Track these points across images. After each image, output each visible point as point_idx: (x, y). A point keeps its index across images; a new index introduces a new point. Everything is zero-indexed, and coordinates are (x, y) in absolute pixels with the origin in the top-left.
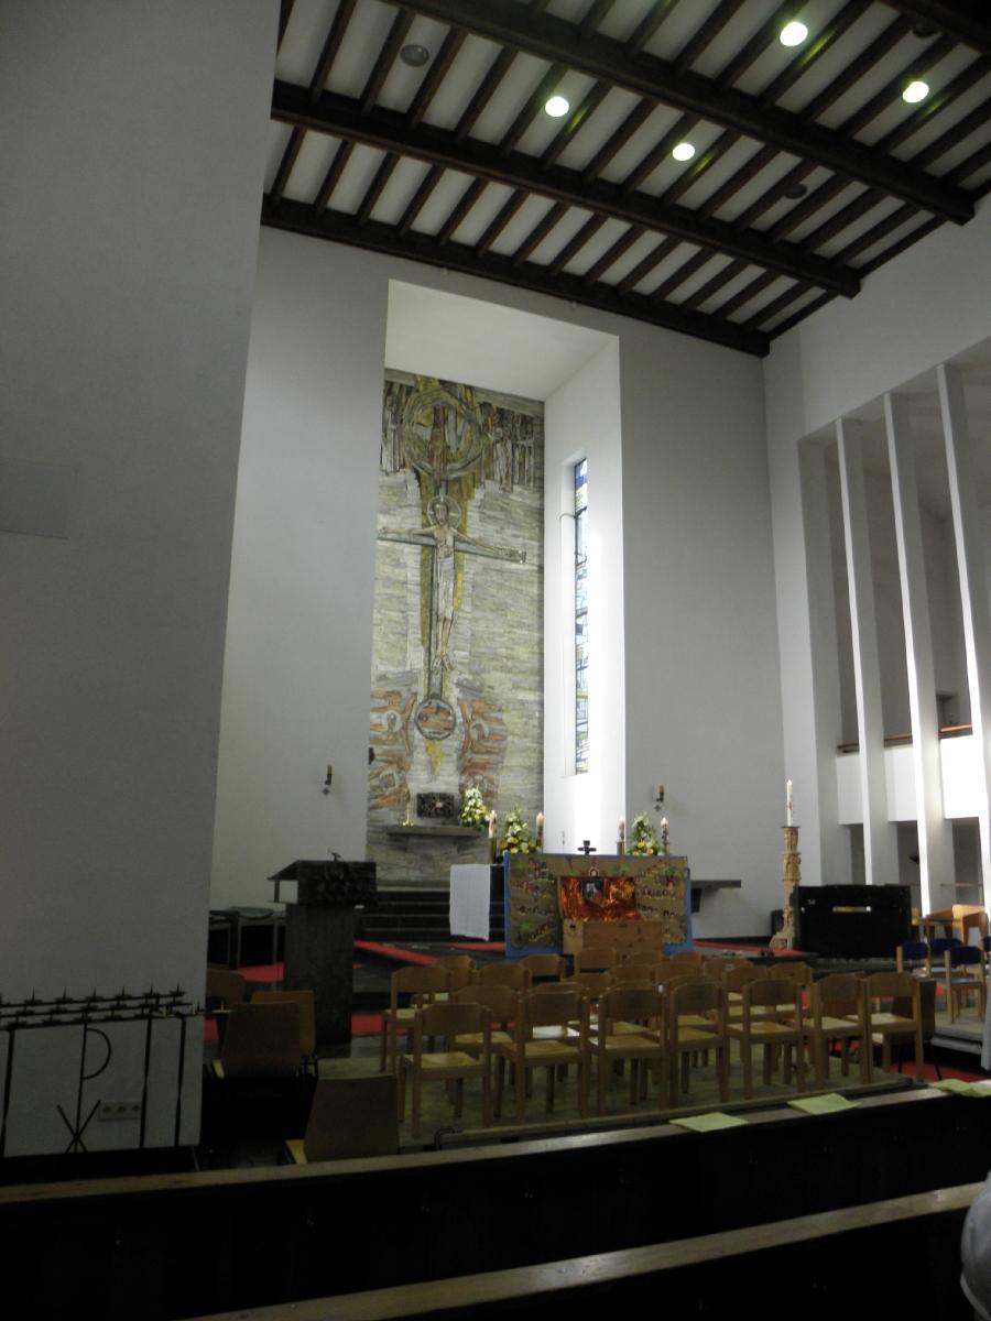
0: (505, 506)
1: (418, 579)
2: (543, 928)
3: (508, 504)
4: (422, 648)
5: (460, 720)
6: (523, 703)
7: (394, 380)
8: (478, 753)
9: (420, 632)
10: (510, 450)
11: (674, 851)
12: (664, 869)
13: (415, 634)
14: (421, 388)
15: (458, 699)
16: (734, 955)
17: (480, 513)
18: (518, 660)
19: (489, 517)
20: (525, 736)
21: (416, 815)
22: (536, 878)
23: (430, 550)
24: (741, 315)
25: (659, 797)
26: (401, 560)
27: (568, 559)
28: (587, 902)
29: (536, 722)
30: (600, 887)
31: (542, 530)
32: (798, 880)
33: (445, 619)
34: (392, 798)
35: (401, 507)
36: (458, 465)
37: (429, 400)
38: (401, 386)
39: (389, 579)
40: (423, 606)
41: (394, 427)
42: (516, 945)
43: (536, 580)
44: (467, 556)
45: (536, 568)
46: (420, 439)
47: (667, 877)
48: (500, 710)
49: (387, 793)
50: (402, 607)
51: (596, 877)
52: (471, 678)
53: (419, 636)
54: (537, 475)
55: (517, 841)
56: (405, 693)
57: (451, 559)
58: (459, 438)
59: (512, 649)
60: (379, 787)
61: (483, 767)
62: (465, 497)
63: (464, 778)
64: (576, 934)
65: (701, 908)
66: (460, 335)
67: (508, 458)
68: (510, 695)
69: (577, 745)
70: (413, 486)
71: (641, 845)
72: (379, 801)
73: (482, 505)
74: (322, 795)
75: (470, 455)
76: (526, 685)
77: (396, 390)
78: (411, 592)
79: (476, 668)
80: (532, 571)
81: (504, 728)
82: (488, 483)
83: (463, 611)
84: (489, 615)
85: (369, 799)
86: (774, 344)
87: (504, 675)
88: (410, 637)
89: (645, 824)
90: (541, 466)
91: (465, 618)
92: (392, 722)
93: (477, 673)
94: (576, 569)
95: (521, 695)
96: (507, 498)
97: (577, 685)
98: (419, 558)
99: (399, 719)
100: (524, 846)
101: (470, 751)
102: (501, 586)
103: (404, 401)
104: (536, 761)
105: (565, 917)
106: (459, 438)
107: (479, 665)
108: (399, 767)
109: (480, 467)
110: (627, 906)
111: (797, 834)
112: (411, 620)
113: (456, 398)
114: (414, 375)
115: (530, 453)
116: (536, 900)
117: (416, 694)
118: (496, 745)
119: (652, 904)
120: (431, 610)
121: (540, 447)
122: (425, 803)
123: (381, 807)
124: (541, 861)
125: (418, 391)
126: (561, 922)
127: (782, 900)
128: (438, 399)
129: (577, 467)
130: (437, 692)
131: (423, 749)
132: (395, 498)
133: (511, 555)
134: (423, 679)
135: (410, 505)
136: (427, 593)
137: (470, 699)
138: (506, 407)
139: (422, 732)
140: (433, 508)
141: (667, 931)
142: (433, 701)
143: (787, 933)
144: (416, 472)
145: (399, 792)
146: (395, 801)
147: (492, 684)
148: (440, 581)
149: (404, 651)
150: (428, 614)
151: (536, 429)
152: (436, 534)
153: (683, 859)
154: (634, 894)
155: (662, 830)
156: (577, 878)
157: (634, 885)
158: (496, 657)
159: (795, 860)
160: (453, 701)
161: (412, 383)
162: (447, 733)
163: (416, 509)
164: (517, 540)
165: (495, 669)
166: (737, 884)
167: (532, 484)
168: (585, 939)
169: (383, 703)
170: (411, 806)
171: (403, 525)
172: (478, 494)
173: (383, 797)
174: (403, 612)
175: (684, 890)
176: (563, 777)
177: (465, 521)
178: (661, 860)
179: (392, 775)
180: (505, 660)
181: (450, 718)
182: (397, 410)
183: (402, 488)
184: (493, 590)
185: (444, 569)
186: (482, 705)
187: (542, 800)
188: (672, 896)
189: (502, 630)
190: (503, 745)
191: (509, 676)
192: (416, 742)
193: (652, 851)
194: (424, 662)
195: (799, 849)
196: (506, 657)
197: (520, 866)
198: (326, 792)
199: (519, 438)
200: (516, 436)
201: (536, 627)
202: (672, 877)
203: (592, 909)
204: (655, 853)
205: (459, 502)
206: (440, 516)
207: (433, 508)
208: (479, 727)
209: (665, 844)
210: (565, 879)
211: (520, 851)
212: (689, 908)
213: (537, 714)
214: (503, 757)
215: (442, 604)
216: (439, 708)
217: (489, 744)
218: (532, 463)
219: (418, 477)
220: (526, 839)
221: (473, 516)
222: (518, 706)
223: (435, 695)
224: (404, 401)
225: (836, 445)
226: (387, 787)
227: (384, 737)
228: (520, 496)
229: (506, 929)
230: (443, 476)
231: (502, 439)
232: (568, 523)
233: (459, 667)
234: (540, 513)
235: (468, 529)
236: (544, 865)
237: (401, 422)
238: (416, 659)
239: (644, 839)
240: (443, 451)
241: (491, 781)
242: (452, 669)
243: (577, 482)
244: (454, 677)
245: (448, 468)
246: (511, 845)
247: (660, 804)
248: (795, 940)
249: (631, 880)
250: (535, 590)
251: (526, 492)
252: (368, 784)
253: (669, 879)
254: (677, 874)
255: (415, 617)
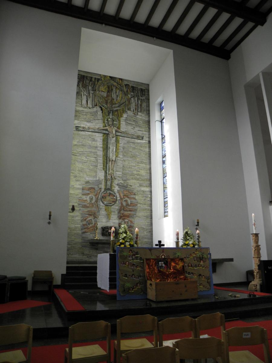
0: (135, 120)
1: (102, 146)
2: (137, 286)
3: (136, 119)
4: (103, 171)
5: (119, 198)
6: (143, 191)
7: (93, 76)
8: (126, 211)
9: (102, 165)
10: (136, 100)
11: (203, 245)
12: (199, 254)
13: (100, 166)
14: (103, 79)
15: (118, 190)
16: (235, 297)
17: (125, 122)
18: (142, 176)
19: (129, 124)
20: (145, 204)
21: (101, 235)
22: (133, 260)
23: (106, 136)
24: (219, 42)
25: (197, 224)
26: (95, 139)
27: (158, 136)
28: (159, 271)
29: (149, 199)
30: (166, 263)
31: (149, 128)
32: (260, 257)
33: (112, 160)
34: (91, 229)
35: (95, 120)
36: (117, 105)
37: (106, 83)
38: (95, 78)
39: (90, 146)
40: (104, 156)
41: (93, 92)
42: (122, 294)
43: (148, 146)
44: (120, 137)
45: (148, 142)
46: (102, 96)
47: (200, 258)
48: (135, 194)
49: (89, 227)
50: (95, 156)
51: (164, 259)
52: (123, 182)
53: (102, 167)
54: (147, 109)
55: (124, 242)
56: (96, 187)
57: (114, 138)
58: (117, 96)
59: (139, 171)
60: (86, 225)
61: (128, 216)
62: (120, 116)
63: (120, 221)
64: (152, 288)
65: (217, 270)
66: (115, 55)
67: (136, 103)
68: (139, 189)
69: (164, 206)
70: (100, 113)
71: (187, 243)
72: (86, 230)
73: (126, 119)
74: (48, 224)
75: (122, 102)
76: (144, 185)
77: (93, 80)
78: (99, 150)
79: (125, 178)
80: (146, 143)
81: (136, 201)
82: (129, 112)
83: (119, 157)
84: (129, 159)
85: (82, 229)
86: (233, 55)
87: (136, 181)
88: (99, 167)
89: (189, 233)
90: (148, 106)
91: (120, 160)
92: (91, 199)
93: (125, 180)
94: (162, 140)
95: (143, 189)
96: (136, 117)
97: (164, 183)
98: (102, 138)
99: (94, 198)
100: (127, 244)
101: (123, 210)
102: (134, 148)
103: (96, 83)
104: (149, 214)
105: (148, 279)
106: (117, 96)
107: (126, 177)
108: (94, 216)
109: (126, 106)
110: (183, 271)
111: (258, 237)
112: (99, 161)
113: (116, 82)
114: (100, 75)
115: (144, 101)
116: (133, 271)
117: (101, 188)
118: (133, 208)
119: (191, 271)
120: (107, 157)
121: (148, 99)
122: (105, 231)
123: (87, 232)
124: (136, 251)
125: (102, 80)
126: (146, 282)
127: (254, 266)
128: (109, 83)
129: (161, 104)
130: (109, 188)
131: (104, 210)
132: (93, 117)
133: (138, 137)
134: (103, 183)
135: (99, 119)
136: (105, 151)
137: (122, 190)
138: (135, 86)
139: (103, 203)
140: (107, 120)
141: (201, 284)
142: (108, 191)
143: (256, 282)
144: (101, 108)
145: (94, 226)
146: (92, 230)
147: (131, 185)
148: (111, 146)
149: (96, 172)
150: (106, 158)
151: (146, 93)
152: (108, 130)
153: (208, 249)
154: (183, 266)
155: (197, 235)
156: (155, 259)
157: (184, 262)
158: (133, 175)
159: (258, 248)
160: (116, 191)
161: (99, 78)
162: (113, 203)
163: (101, 120)
164: (137, 131)
165: (132, 179)
166: (231, 260)
167: (145, 112)
168: (156, 292)
169: (88, 192)
170: (99, 231)
171: (96, 126)
172: (125, 116)
173: (88, 228)
174: (96, 158)
175: (209, 263)
176: (159, 219)
177: (120, 125)
178: (196, 250)
179: (91, 220)
180: (136, 176)
181: (115, 198)
182: (93, 86)
183: (95, 113)
184: (131, 150)
185: (112, 142)
186: (127, 192)
187: (152, 229)
188: (203, 267)
189: (134, 164)
190: (135, 208)
191: (138, 181)
192: (101, 207)
193: (192, 245)
194: (104, 176)
195: (259, 244)
196: (136, 174)
197: (125, 254)
198: (49, 223)
199: (140, 96)
200: (139, 96)
201: (148, 163)
202: (203, 258)
203: (163, 275)
204: (194, 246)
205: (117, 118)
206: (110, 123)
207: (107, 120)
208: (126, 201)
209: (199, 242)
210: (148, 260)
211: (125, 246)
212: (211, 272)
213: (149, 196)
214: (136, 212)
215: (111, 155)
216: (110, 194)
217: (131, 207)
218: (145, 105)
219: (102, 110)
220: (128, 240)
221: (123, 123)
222: (141, 193)
223: (108, 189)
224: (96, 83)
225: (260, 85)
226: (89, 224)
227: (88, 205)
228: (141, 116)
229: (117, 283)
230: (111, 109)
231: (133, 97)
232: (158, 124)
233: (118, 178)
234: (149, 122)
235: (121, 128)
236: (137, 253)
237: (95, 90)
238: (101, 175)
239: (188, 240)
240: (111, 100)
241: (131, 222)
242: (115, 179)
243: (161, 109)
244: (116, 182)
245: (113, 106)
246: (121, 243)
247: (197, 227)
248: (261, 286)
249: (182, 260)
250: (147, 150)
251: (143, 115)
252: (81, 224)
253: (201, 259)
254: (205, 256)
255: (101, 160)
